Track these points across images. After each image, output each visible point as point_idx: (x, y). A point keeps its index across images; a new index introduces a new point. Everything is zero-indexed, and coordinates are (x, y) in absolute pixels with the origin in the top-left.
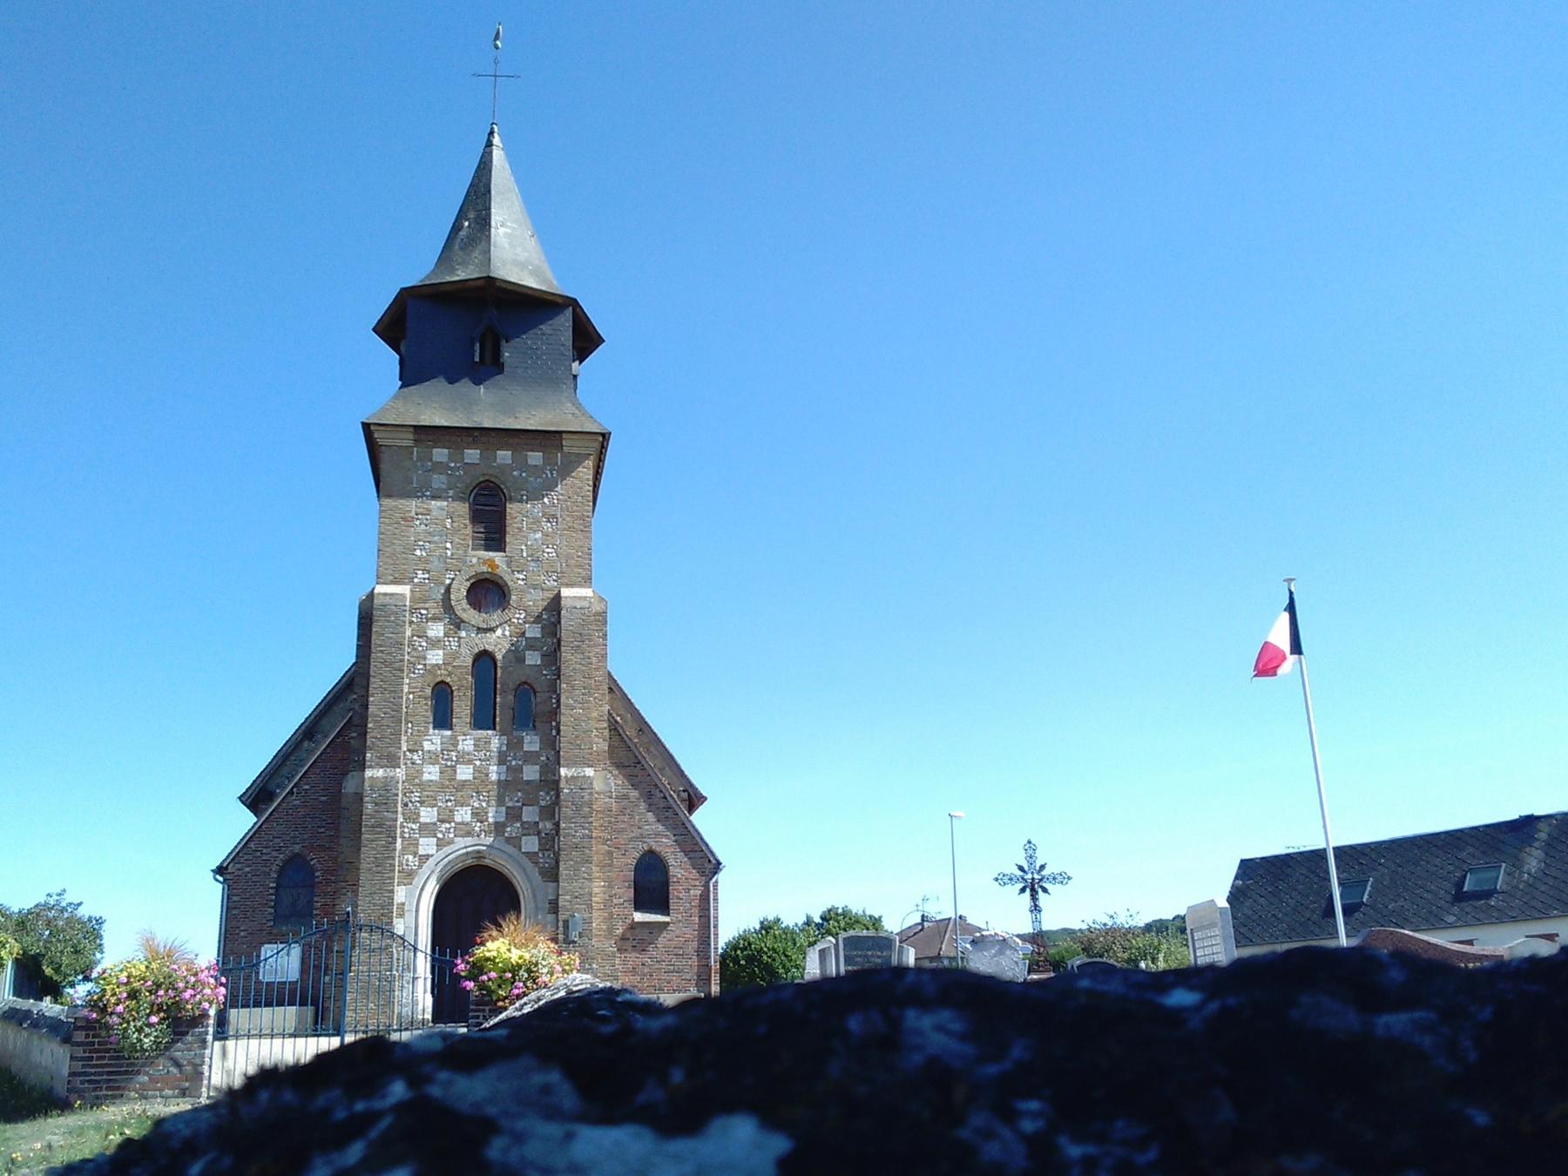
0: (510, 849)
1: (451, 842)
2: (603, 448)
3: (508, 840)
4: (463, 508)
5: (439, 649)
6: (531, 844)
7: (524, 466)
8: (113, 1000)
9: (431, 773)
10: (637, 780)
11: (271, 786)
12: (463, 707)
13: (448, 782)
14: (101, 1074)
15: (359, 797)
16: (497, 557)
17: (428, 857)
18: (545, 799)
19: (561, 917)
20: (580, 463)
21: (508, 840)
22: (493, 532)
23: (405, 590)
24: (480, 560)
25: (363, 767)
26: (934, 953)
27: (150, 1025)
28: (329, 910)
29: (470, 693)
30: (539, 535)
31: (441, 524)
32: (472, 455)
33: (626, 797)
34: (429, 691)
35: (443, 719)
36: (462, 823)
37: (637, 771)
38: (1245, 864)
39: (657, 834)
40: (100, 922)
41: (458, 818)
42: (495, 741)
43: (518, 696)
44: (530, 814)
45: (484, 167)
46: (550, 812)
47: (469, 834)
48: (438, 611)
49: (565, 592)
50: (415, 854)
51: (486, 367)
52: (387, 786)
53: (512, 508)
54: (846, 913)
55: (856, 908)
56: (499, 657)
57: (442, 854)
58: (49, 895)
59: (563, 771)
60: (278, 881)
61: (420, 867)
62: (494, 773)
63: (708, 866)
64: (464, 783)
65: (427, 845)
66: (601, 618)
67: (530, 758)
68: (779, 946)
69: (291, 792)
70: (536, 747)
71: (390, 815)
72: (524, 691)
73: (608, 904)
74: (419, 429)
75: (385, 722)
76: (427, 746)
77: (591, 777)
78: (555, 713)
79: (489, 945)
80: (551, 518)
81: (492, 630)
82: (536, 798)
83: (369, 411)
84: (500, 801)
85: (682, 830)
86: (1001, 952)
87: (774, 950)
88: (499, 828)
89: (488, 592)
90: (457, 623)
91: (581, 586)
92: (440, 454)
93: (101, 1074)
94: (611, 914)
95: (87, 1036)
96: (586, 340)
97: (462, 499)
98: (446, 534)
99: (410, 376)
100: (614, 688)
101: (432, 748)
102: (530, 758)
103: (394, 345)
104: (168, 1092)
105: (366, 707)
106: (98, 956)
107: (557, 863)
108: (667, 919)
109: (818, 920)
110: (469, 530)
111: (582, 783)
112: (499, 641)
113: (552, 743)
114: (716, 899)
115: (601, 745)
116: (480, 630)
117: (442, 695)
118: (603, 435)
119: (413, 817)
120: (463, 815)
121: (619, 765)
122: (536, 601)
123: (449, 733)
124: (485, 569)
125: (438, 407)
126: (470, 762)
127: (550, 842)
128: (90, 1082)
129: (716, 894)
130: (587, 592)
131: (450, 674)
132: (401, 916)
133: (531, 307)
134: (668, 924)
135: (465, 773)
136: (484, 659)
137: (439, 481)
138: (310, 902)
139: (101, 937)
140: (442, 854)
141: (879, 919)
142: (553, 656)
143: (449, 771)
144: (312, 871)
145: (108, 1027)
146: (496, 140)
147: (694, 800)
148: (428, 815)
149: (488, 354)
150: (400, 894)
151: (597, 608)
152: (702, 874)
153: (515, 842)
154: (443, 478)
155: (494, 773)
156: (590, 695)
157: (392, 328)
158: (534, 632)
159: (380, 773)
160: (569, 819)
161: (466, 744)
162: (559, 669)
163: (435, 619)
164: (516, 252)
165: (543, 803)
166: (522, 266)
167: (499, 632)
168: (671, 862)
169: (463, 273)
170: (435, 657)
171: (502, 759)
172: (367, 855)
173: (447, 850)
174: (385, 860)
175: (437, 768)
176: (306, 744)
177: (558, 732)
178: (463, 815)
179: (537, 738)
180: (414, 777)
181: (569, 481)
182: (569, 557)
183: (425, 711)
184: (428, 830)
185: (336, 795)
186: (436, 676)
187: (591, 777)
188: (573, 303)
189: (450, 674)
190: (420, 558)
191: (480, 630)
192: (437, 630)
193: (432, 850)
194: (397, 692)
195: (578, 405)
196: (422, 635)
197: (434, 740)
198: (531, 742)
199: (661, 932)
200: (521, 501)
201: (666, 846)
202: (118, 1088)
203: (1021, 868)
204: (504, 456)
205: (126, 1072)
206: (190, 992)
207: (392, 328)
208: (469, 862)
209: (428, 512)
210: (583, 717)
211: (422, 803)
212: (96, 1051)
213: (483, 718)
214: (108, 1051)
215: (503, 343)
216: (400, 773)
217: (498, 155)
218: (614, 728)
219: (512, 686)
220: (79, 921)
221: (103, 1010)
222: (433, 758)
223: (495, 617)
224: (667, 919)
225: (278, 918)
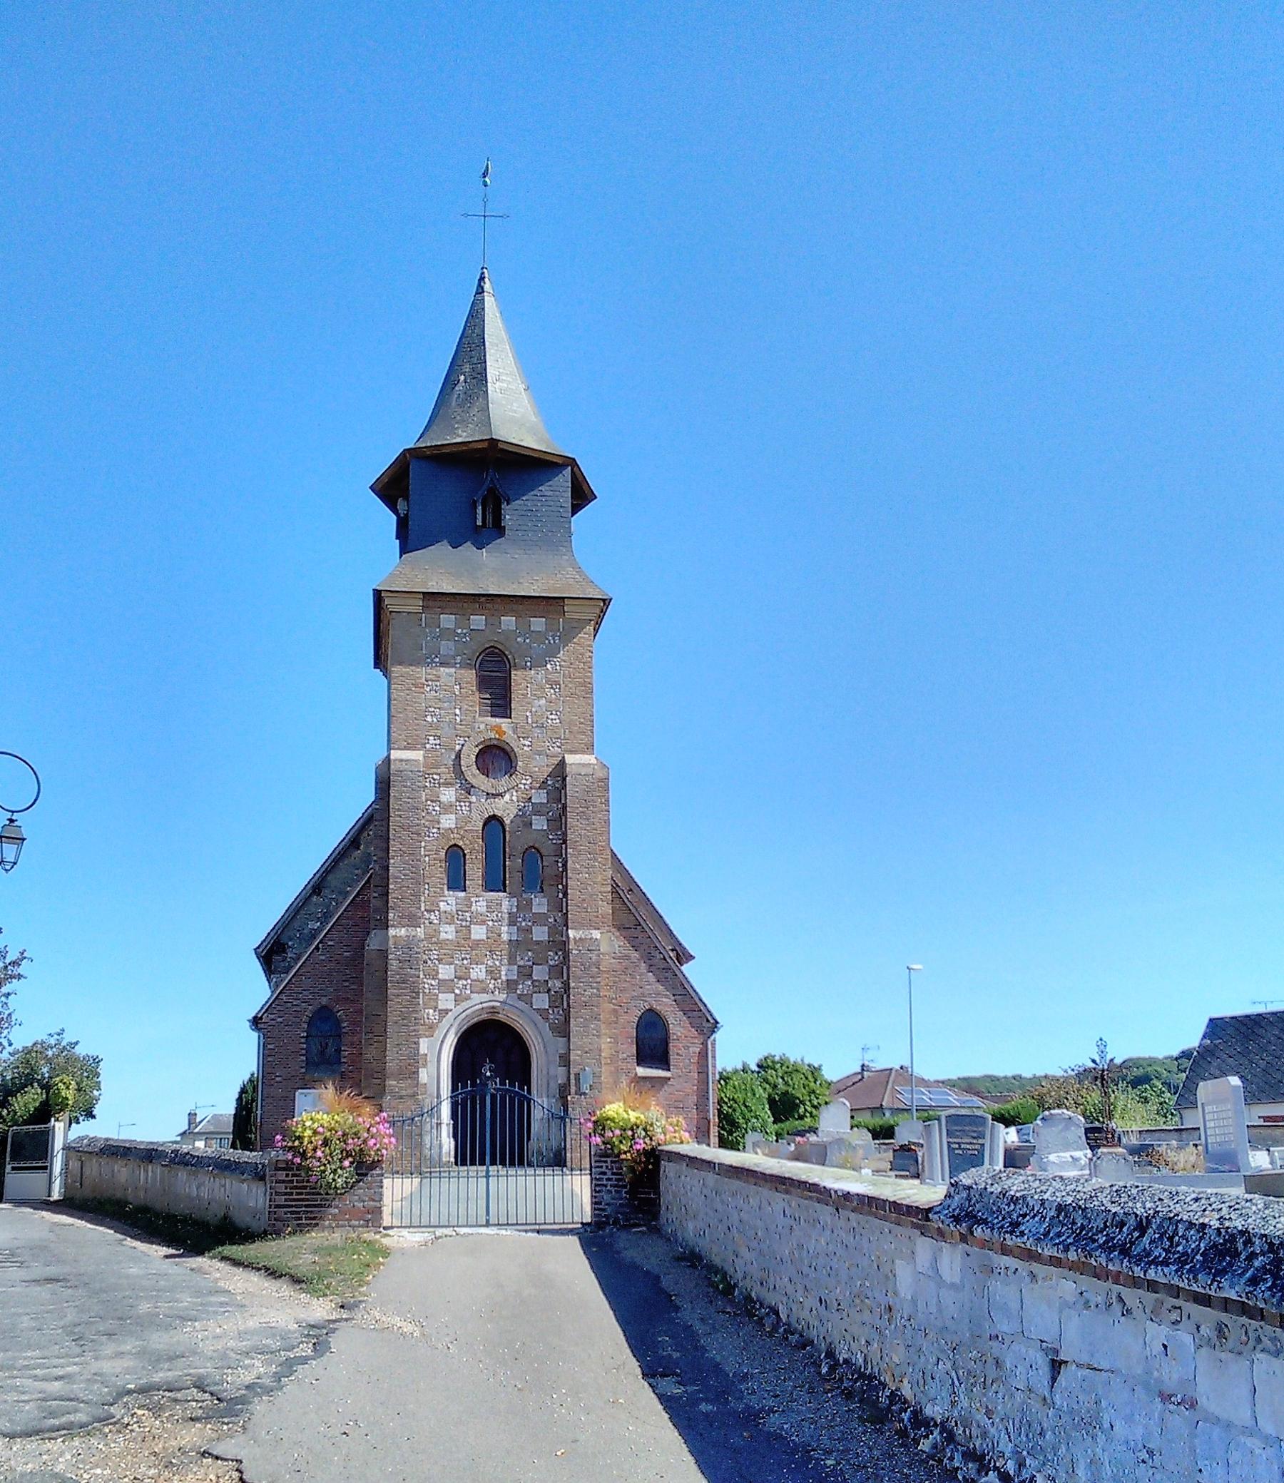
0: (521, 1005)
1: (468, 998)
2: (603, 612)
3: (520, 997)
4: (471, 675)
5: (450, 814)
6: (542, 1001)
9: (448, 933)
12: (475, 870)
13: (465, 942)
14: (301, 1206)
15: (384, 954)
16: (504, 723)
17: (447, 1011)
21: (520, 997)
23: (418, 755)
24: (488, 727)
29: (481, 856)
30: (543, 702)
31: (448, 691)
32: (478, 621)
34: (443, 854)
35: (457, 881)
37: (637, 933)
40: (97, 1061)
41: (473, 975)
42: (506, 903)
43: (529, 860)
44: (540, 973)
45: (476, 315)
46: (561, 970)
47: (484, 991)
49: (570, 759)
51: (489, 530)
52: (409, 944)
53: (516, 675)
55: (793, 1057)
56: (507, 822)
59: (571, 933)
61: (440, 1021)
62: (506, 933)
63: (706, 1025)
64: (477, 943)
65: (446, 1001)
66: (604, 785)
67: (538, 919)
68: (739, 1096)
69: (317, 948)
71: (413, 972)
72: (532, 854)
73: (613, 1059)
74: (428, 596)
77: (595, 938)
80: (554, 684)
81: (501, 795)
82: (548, 959)
84: (512, 961)
86: (1067, 1128)
88: (510, 985)
89: (496, 757)
90: (468, 789)
91: (583, 752)
92: (448, 620)
93: (301, 1206)
95: (287, 1175)
96: (581, 495)
97: (469, 666)
99: (408, 538)
100: (614, 855)
101: (448, 908)
102: (538, 919)
105: (387, 869)
106: (95, 1092)
109: (755, 1068)
111: (591, 946)
112: (507, 807)
113: (560, 906)
114: (714, 1057)
117: (455, 857)
118: (604, 600)
120: (478, 972)
121: (621, 928)
122: (542, 766)
123: (462, 894)
125: (445, 569)
126: (483, 922)
128: (291, 1213)
129: (714, 1051)
132: (425, 1066)
133: (527, 467)
135: (478, 933)
137: (446, 647)
138: (339, 1051)
139: (98, 1075)
140: (460, 1009)
141: (819, 1069)
142: (559, 821)
144: (338, 1022)
146: (487, 286)
147: (683, 956)
148: (446, 972)
150: (424, 1046)
151: (601, 774)
152: (701, 1032)
154: (451, 644)
155: (506, 933)
156: (596, 860)
157: (392, 488)
158: (540, 797)
159: (403, 932)
160: (578, 979)
161: (480, 906)
162: (565, 834)
163: (447, 784)
164: (514, 410)
165: (551, 963)
167: (507, 797)
169: (463, 435)
170: (448, 821)
172: (394, 1007)
173: (465, 1005)
174: (410, 1017)
177: (565, 894)
178: (478, 972)
179: (545, 901)
180: (432, 936)
181: (570, 647)
182: (571, 723)
183: (439, 872)
184: (446, 986)
185: (360, 950)
186: (449, 839)
187: (595, 938)
188: (572, 462)
189: (463, 837)
192: (448, 795)
193: (451, 1005)
195: (579, 570)
197: (450, 901)
198: (540, 904)
200: (525, 668)
202: (314, 1218)
203: (1094, 1061)
204: (509, 622)
205: (320, 1206)
206: (373, 1141)
210: (587, 883)
212: (296, 1187)
213: (494, 882)
214: (305, 1187)
216: (420, 932)
218: (615, 890)
219: (520, 849)
220: (77, 1059)
223: (503, 782)
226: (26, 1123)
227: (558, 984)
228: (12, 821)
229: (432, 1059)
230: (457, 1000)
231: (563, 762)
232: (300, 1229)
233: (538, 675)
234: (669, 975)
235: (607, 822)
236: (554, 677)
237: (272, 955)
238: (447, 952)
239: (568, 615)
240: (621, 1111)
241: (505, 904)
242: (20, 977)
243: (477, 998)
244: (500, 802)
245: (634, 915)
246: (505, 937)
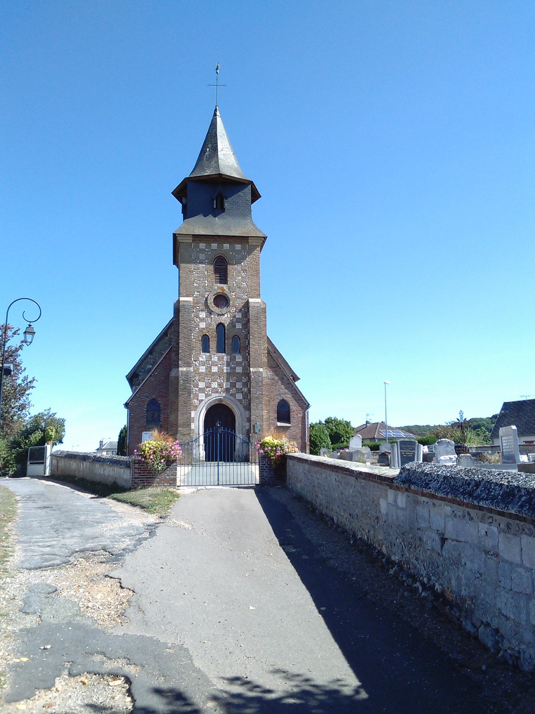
1: (211, 395)
4: (211, 267)
5: (203, 322)
6: (239, 396)
7: (234, 250)
8: (148, 454)
9: (202, 369)
10: (278, 372)
11: (137, 372)
12: (213, 344)
15: (177, 378)
16: (225, 286)
17: (202, 400)
18: (244, 380)
19: (252, 424)
20: (255, 249)
22: (223, 278)
23: (190, 299)
24: (218, 287)
25: (178, 367)
26: (372, 437)
27: (161, 463)
28: (167, 419)
30: (240, 278)
31: (202, 273)
32: (214, 246)
33: (273, 379)
34: (200, 338)
35: (206, 349)
36: (214, 388)
38: (505, 404)
39: (286, 393)
40: (64, 420)
41: (213, 386)
42: (225, 358)
43: (236, 339)
44: (239, 385)
46: (247, 384)
47: (217, 392)
48: (203, 307)
49: (251, 300)
50: (197, 399)
51: (218, 210)
52: (187, 373)
53: (230, 267)
54: (335, 420)
56: (226, 325)
57: (207, 399)
58: (45, 410)
59: (251, 369)
60: (147, 408)
61: (199, 404)
63: (304, 405)
64: (214, 373)
65: (202, 396)
66: (264, 311)
68: (318, 434)
70: (241, 360)
71: (189, 385)
72: (236, 338)
73: (268, 419)
74: (194, 236)
75: (186, 350)
76: (200, 359)
77: (261, 371)
78: (247, 346)
79: (266, 438)
80: (244, 271)
81: (223, 315)
82: (241, 379)
83: (175, 229)
85: (294, 392)
86: (447, 446)
87: (316, 436)
88: (227, 390)
89: (222, 300)
90: (210, 312)
91: (256, 298)
92: (202, 246)
94: (269, 423)
96: (255, 196)
98: (205, 277)
99: (187, 213)
103: (180, 200)
104: (166, 484)
106: (63, 433)
107: (250, 404)
108: (289, 425)
109: (324, 423)
110: (214, 276)
111: (259, 374)
112: (226, 319)
113: (247, 358)
114: (308, 418)
115: (265, 360)
116: (219, 315)
117: (205, 339)
118: (264, 238)
119: (197, 386)
120: (215, 385)
121: (271, 367)
122: (239, 303)
123: (208, 354)
124: (220, 291)
125: (201, 226)
126: (216, 365)
127: (247, 396)
128: (141, 480)
129: (308, 416)
130: (258, 300)
131: (208, 332)
134: (290, 427)
135: (215, 369)
136: (220, 325)
137: (202, 256)
138: (159, 416)
139: (64, 426)
140: (207, 399)
142: (246, 325)
143: (209, 369)
144: (159, 405)
145: (147, 463)
146: (218, 113)
148: (202, 385)
149: (219, 207)
150: (193, 414)
151: (263, 306)
152: (302, 408)
153: (233, 395)
154: (204, 255)
157: (180, 193)
158: (239, 316)
159: (184, 369)
160: (254, 388)
161: (215, 358)
162: (249, 330)
163: (202, 310)
164: (228, 162)
165: (243, 381)
166: (231, 167)
167: (226, 316)
168: (291, 404)
170: (203, 325)
171: (228, 365)
172: (181, 399)
173: (209, 398)
175: (204, 367)
176: (150, 356)
177: (249, 354)
178: (215, 385)
179: (241, 357)
180: (196, 371)
181: (251, 256)
182: (251, 286)
183: (199, 345)
184: (202, 390)
185: (167, 377)
187: (261, 371)
188: (251, 183)
189: (208, 332)
190: (196, 287)
191: (219, 315)
192: (203, 315)
193: (204, 398)
194: (189, 339)
195: (254, 225)
196: (197, 317)
197: (203, 357)
198: (239, 358)
199: (287, 430)
201: (289, 397)
202: (150, 483)
203: (458, 419)
204: (226, 246)
207: (180, 193)
208: (217, 402)
209: (198, 268)
210: (257, 349)
211: (199, 380)
212: (142, 471)
213: (221, 349)
214: (146, 470)
215: (225, 200)
216: (192, 369)
217: (219, 120)
218: (269, 353)
221: (145, 458)
222: (203, 364)
223: (225, 310)
224: (289, 425)
225: (148, 422)
226: (36, 445)
227: (246, 389)
228: (30, 325)
230: (207, 396)
232: (144, 487)
233: (238, 267)
236: (244, 268)
237: (133, 378)
239: (250, 244)
243: (214, 395)
246: (225, 371)
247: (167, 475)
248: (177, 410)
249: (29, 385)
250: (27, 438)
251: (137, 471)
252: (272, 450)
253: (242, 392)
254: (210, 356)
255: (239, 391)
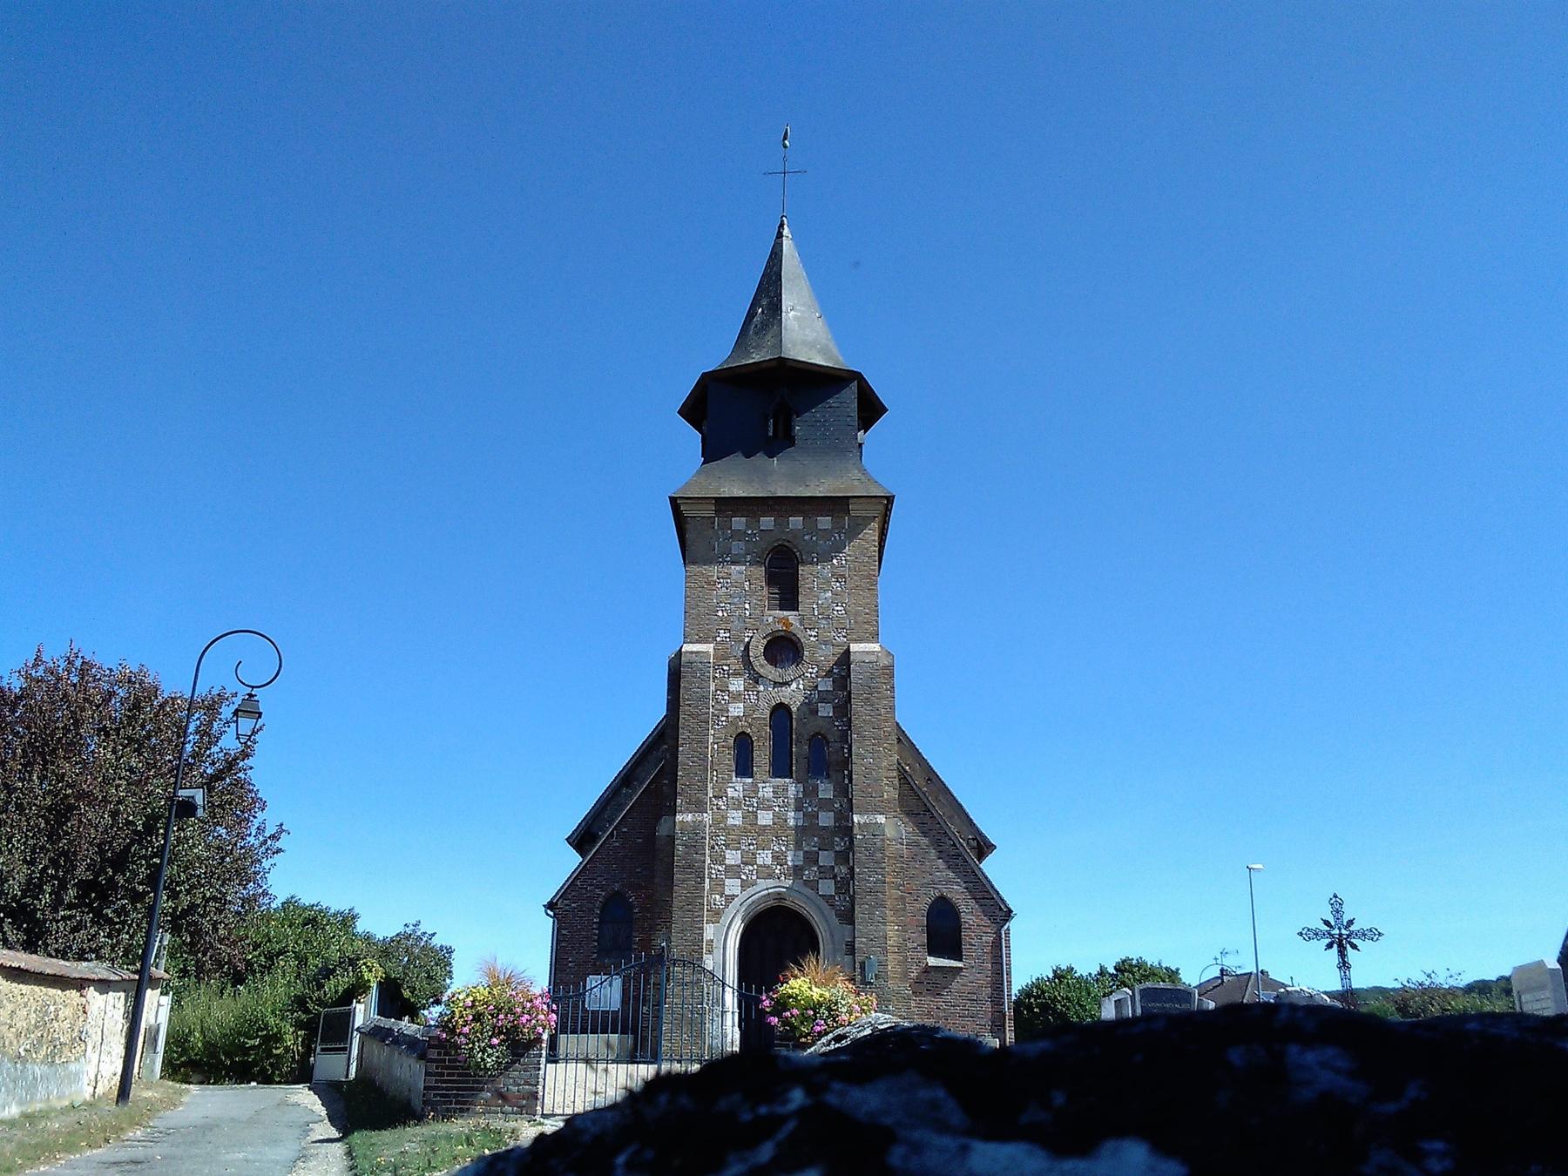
0: (808, 891)
1: (754, 884)
4: (760, 572)
5: (739, 703)
6: (827, 887)
7: (814, 531)
9: (735, 818)
12: (762, 756)
15: (671, 839)
16: (791, 616)
17: (733, 897)
22: (788, 596)
23: (709, 648)
24: (775, 618)
27: (492, 1047)
28: (647, 945)
31: (739, 586)
32: (767, 522)
35: (744, 767)
39: (948, 881)
40: (450, 951)
43: (813, 747)
44: (826, 859)
46: (844, 857)
47: (770, 876)
49: (854, 647)
51: (779, 442)
52: (697, 828)
54: (1141, 965)
56: (794, 709)
59: (856, 818)
62: (792, 818)
63: (1000, 913)
65: (732, 886)
66: (889, 671)
67: (825, 805)
72: (818, 741)
73: (901, 948)
77: (881, 823)
78: (847, 762)
79: (792, 982)
80: (839, 577)
81: (788, 684)
82: (831, 843)
84: (798, 846)
88: (797, 871)
89: (784, 648)
90: (756, 678)
92: (739, 522)
96: (870, 410)
97: (758, 563)
98: (745, 595)
99: (711, 453)
100: (902, 739)
102: (825, 805)
108: (960, 965)
109: (1112, 971)
112: (794, 694)
113: (844, 791)
115: (890, 793)
116: (776, 684)
117: (743, 745)
118: (887, 498)
120: (765, 858)
122: (827, 656)
125: (735, 480)
126: (769, 808)
128: (442, 1096)
129: (1008, 941)
130: (875, 647)
131: (750, 725)
133: (819, 383)
135: (765, 818)
136: (780, 711)
137: (737, 547)
142: (843, 710)
143: (750, 817)
145: (457, 1047)
146: (786, 231)
147: (983, 848)
148: (733, 857)
150: (709, 932)
151: (885, 662)
153: (813, 885)
157: (694, 410)
158: (826, 685)
159: (689, 817)
161: (766, 791)
163: (737, 674)
164: (805, 334)
167: (794, 685)
168: (962, 908)
170: (737, 710)
172: (680, 893)
173: (751, 890)
177: (851, 780)
180: (719, 822)
181: (856, 542)
182: (857, 614)
183: (729, 759)
184: (733, 871)
187: (881, 823)
188: (857, 376)
189: (750, 725)
191: (776, 684)
192: (737, 685)
194: (703, 742)
195: (864, 471)
197: (737, 788)
198: (826, 790)
201: (957, 893)
202: (464, 1103)
203: (1327, 923)
204: (796, 522)
205: (472, 1089)
207: (694, 410)
210: (873, 766)
212: (447, 1068)
213: (781, 768)
214: (456, 1068)
216: (707, 818)
218: (903, 777)
223: (791, 672)
224: (960, 965)
225: (603, 951)
226: (334, 1004)
227: (844, 870)
228: (251, 695)
229: (718, 944)
230: (745, 885)
231: (848, 652)
232: (446, 1116)
233: (824, 570)
234: (960, 861)
235: (892, 708)
236: (840, 571)
237: (581, 840)
238: (734, 838)
239: (862, 515)
240: (805, 987)
241: (792, 789)
242: (279, 851)
243: (763, 884)
244: (787, 691)
245: (927, 800)
246: (791, 822)
247: (511, 1083)
248: (668, 922)
249: (272, 843)
250: (320, 986)
251: (433, 1068)
252: (804, 1019)
253: (835, 877)
254: (754, 785)
255: (827, 873)
